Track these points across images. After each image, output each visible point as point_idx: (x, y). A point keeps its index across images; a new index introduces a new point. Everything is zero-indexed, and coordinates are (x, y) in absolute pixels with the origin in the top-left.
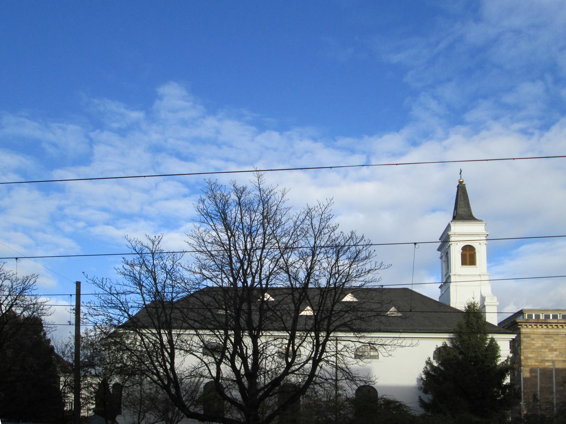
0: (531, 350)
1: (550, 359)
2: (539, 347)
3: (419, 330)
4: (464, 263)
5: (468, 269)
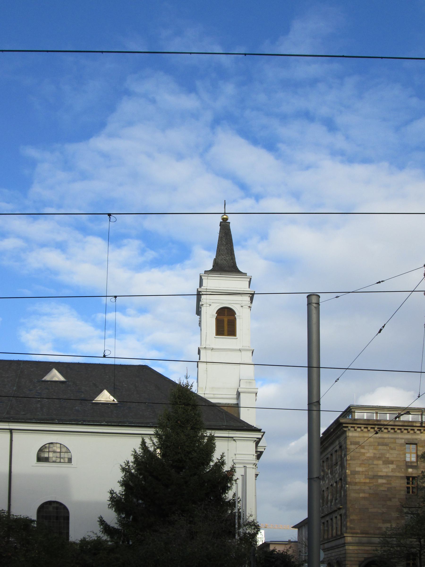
0: (359, 462)
1: (384, 474)
2: (370, 458)
3: (132, 422)
4: (220, 332)
5: (225, 342)
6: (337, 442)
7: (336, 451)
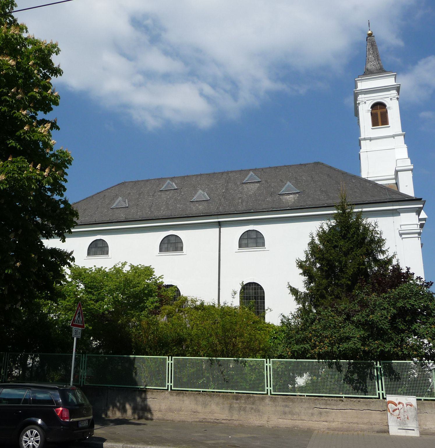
4: (375, 123)
5: (381, 131)
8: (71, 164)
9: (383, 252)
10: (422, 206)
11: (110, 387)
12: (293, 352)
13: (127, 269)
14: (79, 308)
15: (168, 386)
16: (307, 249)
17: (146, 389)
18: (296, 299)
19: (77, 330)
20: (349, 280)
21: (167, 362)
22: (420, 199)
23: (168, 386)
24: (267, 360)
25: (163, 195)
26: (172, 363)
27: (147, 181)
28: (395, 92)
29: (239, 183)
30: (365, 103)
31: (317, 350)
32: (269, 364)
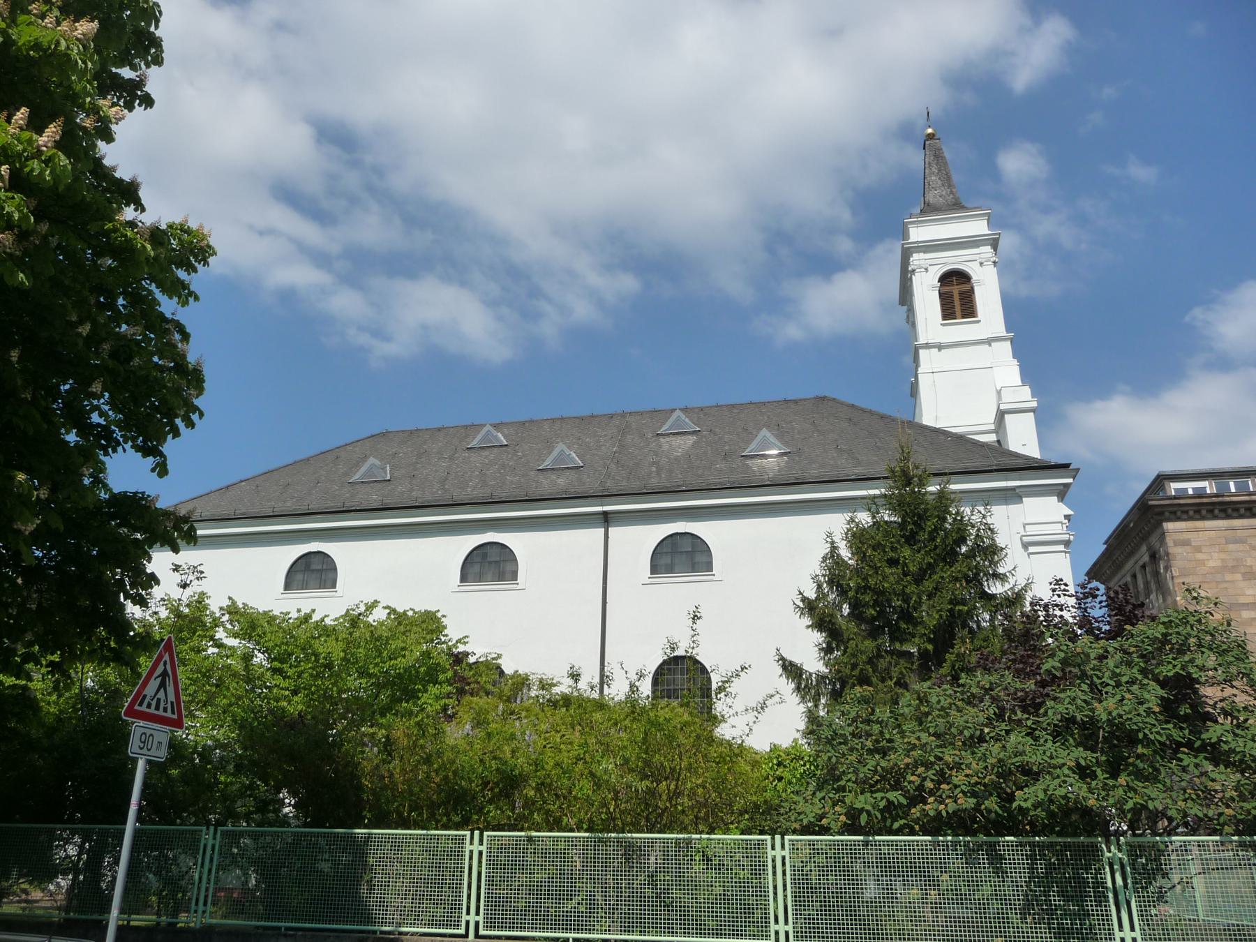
4: (948, 313)
5: (961, 330)
6: (1144, 548)
7: (1144, 567)
8: (206, 263)
9: (1002, 578)
10: (1071, 480)
11: (287, 929)
12: (853, 814)
13: (379, 615)
14: (166, 657)
15: (468, 922)
16: (818, 572)
17: (401, 933)
18: (798, 689)
19: (149, 732)
20: (930, 641)
21: (468, 847)
22: (1066, 466)
23: (468, 922)
24: (773, 839)
25: (475, 458)
26: (480, 853)
27: (439, 430)
28: (988, 249)
29: (650, 435)
30: (926, 270)
31: (931, 807)
32: (779, 851)
